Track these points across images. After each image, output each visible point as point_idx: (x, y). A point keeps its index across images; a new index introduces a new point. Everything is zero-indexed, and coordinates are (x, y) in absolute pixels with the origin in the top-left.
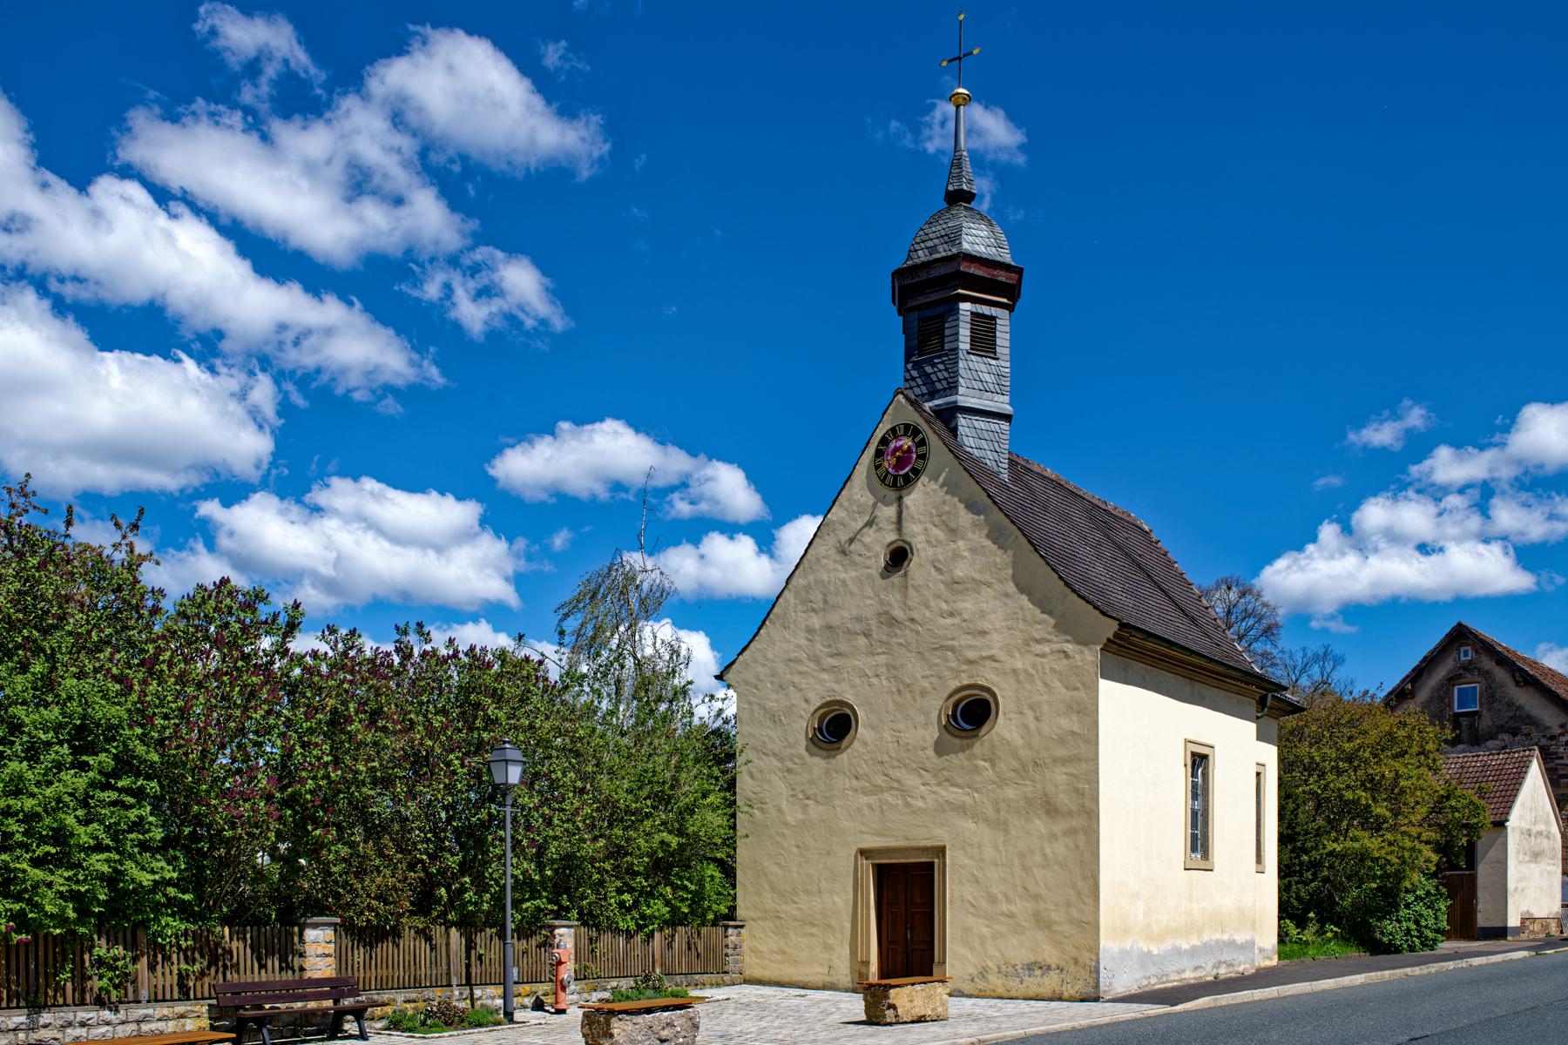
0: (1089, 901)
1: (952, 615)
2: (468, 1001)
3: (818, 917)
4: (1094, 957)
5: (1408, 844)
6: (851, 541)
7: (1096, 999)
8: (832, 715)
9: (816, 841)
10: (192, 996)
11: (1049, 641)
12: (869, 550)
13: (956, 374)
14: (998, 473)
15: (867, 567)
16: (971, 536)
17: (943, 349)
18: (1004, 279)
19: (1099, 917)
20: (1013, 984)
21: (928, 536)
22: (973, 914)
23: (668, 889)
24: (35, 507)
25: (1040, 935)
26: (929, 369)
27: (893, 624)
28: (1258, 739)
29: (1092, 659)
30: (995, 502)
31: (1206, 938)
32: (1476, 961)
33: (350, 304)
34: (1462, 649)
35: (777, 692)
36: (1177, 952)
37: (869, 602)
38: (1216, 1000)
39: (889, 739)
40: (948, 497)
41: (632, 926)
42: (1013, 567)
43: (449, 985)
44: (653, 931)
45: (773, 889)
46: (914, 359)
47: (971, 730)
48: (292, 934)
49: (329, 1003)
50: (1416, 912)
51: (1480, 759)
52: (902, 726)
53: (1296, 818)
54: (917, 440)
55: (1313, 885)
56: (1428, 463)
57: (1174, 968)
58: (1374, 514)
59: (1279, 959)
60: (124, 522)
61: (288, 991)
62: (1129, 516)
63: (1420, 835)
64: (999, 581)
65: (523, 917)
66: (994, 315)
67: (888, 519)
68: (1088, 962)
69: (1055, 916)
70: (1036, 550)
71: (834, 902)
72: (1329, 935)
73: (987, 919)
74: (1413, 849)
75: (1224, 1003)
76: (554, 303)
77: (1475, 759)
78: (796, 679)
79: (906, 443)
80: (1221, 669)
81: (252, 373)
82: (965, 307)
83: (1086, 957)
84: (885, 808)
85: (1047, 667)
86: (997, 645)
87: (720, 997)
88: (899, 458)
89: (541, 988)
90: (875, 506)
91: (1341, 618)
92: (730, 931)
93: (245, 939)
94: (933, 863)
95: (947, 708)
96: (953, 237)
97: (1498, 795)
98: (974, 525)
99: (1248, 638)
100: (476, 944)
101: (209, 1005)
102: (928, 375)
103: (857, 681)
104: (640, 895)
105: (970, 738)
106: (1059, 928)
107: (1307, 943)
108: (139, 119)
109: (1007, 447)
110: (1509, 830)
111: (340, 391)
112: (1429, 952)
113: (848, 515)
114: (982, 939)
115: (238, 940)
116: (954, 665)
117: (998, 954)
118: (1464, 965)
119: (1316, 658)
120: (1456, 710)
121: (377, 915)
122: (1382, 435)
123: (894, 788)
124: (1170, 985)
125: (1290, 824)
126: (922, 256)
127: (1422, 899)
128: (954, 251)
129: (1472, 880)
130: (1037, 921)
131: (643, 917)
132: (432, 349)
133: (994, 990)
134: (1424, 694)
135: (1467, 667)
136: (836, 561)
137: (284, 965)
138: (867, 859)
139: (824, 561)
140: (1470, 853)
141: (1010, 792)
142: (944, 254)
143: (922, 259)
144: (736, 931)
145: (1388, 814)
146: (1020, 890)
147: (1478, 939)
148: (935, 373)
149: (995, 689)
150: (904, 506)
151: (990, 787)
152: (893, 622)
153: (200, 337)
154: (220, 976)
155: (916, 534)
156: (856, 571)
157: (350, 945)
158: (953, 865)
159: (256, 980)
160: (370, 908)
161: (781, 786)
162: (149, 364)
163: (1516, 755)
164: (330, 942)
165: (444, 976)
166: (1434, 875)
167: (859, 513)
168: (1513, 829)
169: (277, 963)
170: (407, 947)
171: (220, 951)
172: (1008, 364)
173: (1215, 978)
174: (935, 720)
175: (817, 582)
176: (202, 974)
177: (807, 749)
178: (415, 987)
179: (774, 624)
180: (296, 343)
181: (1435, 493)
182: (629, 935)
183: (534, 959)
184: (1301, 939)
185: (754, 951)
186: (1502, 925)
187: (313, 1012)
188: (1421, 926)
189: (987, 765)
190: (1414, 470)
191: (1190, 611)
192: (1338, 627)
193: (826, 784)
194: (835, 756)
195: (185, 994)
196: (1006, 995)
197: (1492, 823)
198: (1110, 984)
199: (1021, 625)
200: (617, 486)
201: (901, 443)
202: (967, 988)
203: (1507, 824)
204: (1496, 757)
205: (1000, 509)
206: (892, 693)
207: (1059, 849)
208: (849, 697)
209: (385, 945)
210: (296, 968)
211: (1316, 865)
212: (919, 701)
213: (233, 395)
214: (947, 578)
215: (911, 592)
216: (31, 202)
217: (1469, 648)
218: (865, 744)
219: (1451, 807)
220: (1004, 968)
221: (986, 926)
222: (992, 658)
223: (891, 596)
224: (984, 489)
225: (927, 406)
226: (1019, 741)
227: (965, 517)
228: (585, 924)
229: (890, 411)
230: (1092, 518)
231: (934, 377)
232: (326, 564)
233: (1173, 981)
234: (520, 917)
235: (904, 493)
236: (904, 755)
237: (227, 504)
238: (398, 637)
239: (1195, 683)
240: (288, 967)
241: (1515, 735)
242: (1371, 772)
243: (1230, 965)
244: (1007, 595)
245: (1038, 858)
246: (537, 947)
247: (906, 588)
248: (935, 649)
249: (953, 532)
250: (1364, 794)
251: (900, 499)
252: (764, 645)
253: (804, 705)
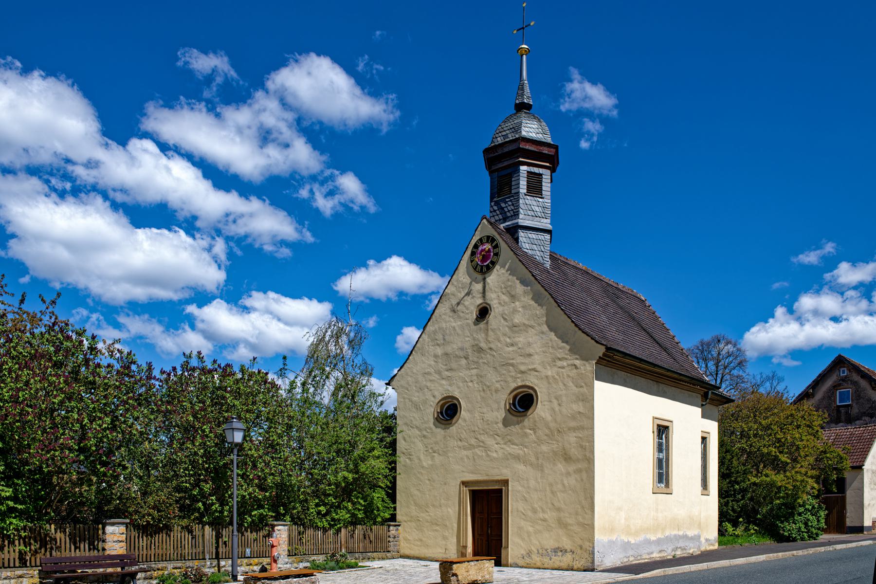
0: (589, 512)
1: (512, 345)
2: (216, 568)
3: (440, 520)
4: (591, 545)
5: (799, 478)
6: (458, 304)
7: (593, 570)
8: (448, 405)
9: (439, 476)
10: (28, 565)
11: (566, 359)
12: (467, 309)
13: (518, 207)
14: (543, 264)
15: (467, 319)
16: (523, 299)
17: (511, 193)
18: (547, 152)
19: (594, 521)
20: (546, 560)
21: (499, 300)
22: (523, 519)
23: (349, 504)
24: (6, 293)
25: (561, 532)
26: (503, 205)
27: (480, 351)
28: (702, 417)
29: (590, 369)
30: (536, 279)
31: (667, 533)
32: (839, 547)
33: (264, 200)
34: (841, 369)
35: (418, 392)
36: (648, 542)
37: (467, 339)
38: (665, 571)
39: (478, 418)
40: (511, 277)
41: (326, 524)
42: (546, 316)
43: (204, 559)
44: (340, 528)
45: (416, 504)
46: (495, 199)
47: (523, 412)
48: (98, 529)
49: (119, 569)
50: (805, 518)
51: (849, 430)
52: (485, 410)
53: (732, 464)
54: (493, 245)
55: (742, 502)
56: (835, 272)
57: (646, 552)
58: (807, 302)
59: (719, 545)
60: (48, 301)
61: (90, 562)
62: (632, 291)
63: (807, 472)
64: (539, 325)
65: (252, 520)
66: (541, 173)
67: (478, 291)
68: (588, 548)
69: (570, 521)
70: (559, 306)
71: (448, 512)
72: (752, 531)
73: (532, 523)
74: (803, 481)
75: (670, 573)
76: (370, 197)
77: (846, 431)
78: (429, 384)
79: (487, 246)
80: (676, 376)
81: (213, 238)
82: (524, 168)
83: (587, 545)
84: (476, 457)
85: (565, 374)
86: (537, 362)
87: (376, 566)
88: (483, 256)
89: (265, 561)
90: (471, 283)
91: (790, 356)
92: (391, 528)
93: (65, 532)
94: (502, 489)
95: (509, 399)
96: (517, 129)
97: (858, 450)
98: (525, 292)
99: (729, 368)
100: (222, 535)
101: (39, 570)
102: (503, 208)
103: (461, 384)
104: (331, 507)
105: (522, 416)
106: (572, 528)
107: (737, 536)
108: (150, 107)
109: (549, 249)
110: (865, 470)
111: (257, 246)
112: (813, 541)
113: (456, 289)
114: (528, 533)
115: (60, 532)
116: (513, 374)
117: (538, 543)
118: (831, 549)
119: (768, 379)
120: (838, 404)
121: (153, 518)
122: (811, 258)
123: (480, 446)
124: (643, 561)
125: (728, 467)
126: (500, 140)
127: (809, 511)
128: (517, 136)
129: (843, 499)
130: (559, 523)
131: (333, 519)
132: (306, 223)
133: (535, 564)
134: (819, 395)
135: (844, 379)
136: (450, 316)
137: (92, 547)
138: (466, 487)
139: (443, 317)
140: (841, 484)
141: (544, 448)
142: (511, 138)
143: (499, 142)
144: (395, 528)
145: (789, 461)
146: (550, 505)
147: (847, 533)
148: (506, 207)
149: (536, 388)
150: (487, 283)
151: (533, 445)
152: (480, 350)
153: (186, 220)
154: (48, 553)
155: (493, 299)
156: (460, 321)
157: (137, 535)
158: (512, 491)
159: (73, 555)
160: (149, 515)
161: (420, 445)
162: (161, 234)
163: (870, 428)
164: (123, 533)
165: (201, 553)
166: (817, 497)
167: (462, 288)
168: (868, 470)
169: (87, 546)
170: (175, 537)
171: (48, 539)
172: (549, 201)
173: (674, 557)
174: (503, 406)
175: (440, 328)
176: (36, 552)
177: (434, 424)
178: (181, 560)
179: (417, 353)
180: (234, 222)
181: (839, 290)
182: (325, 530)
183: (262, 544)
184: (734, 534)
185: (406, 539)
186: (860, 525)
187: (111, 574)
188: (808, 526)
189: (531, 432)
190: (827, 276)
191: (667, 346)
192: (789, 363)
193: (444, 444)
194: (449, 428)
195: (23, 563)
196: (541, 567)
197: (851, 467)
198: (602, 561)
199: (551, 350)
200: (401, 294)
201: (485, 247)
202: (521, 562)
203: (864, 467)
204: (858, 429)
205: (539, 283)
206: (480, 391)
207: (572, 481)
208: (457, 394)
209: (161, 536)
210: (100, 548)
211: (744, 491)
212: (494, 396)
213: (204, 249)
214: (510, 324)
215: (490, 333)
216: (100, 154)
217: (845, 369)
218: (465, 420)
219: (827, 458)
220: (540, 551)
221: (531, 526)
222: (535, 370)
223: (479, 335)
224: (530, 271)
225: (502, 226)
226: (549, 418)
227: (520, 288)
228: (295, 524)
229: (479, 229)
230: (605, 291)
231: (506, 210)
232: (252, 337)
233: (645, 558)
234: (250, 520)
235: (486, 275)
236: (486, 427)
237: (200, 306)
238: (185, 360)
239: (660, 384)
240: (94, 549)
241: (872, 417)
242: (779, 437)
243: (683, 549)
244: (543, 333)
245: (560, 486)
246: (263, 537)
247: (487, 330)
248: (504, 365)
249: (513, 297)
250: (774, 449)
251: (484, 279)
252: (412, 366)
253: (432, 399)
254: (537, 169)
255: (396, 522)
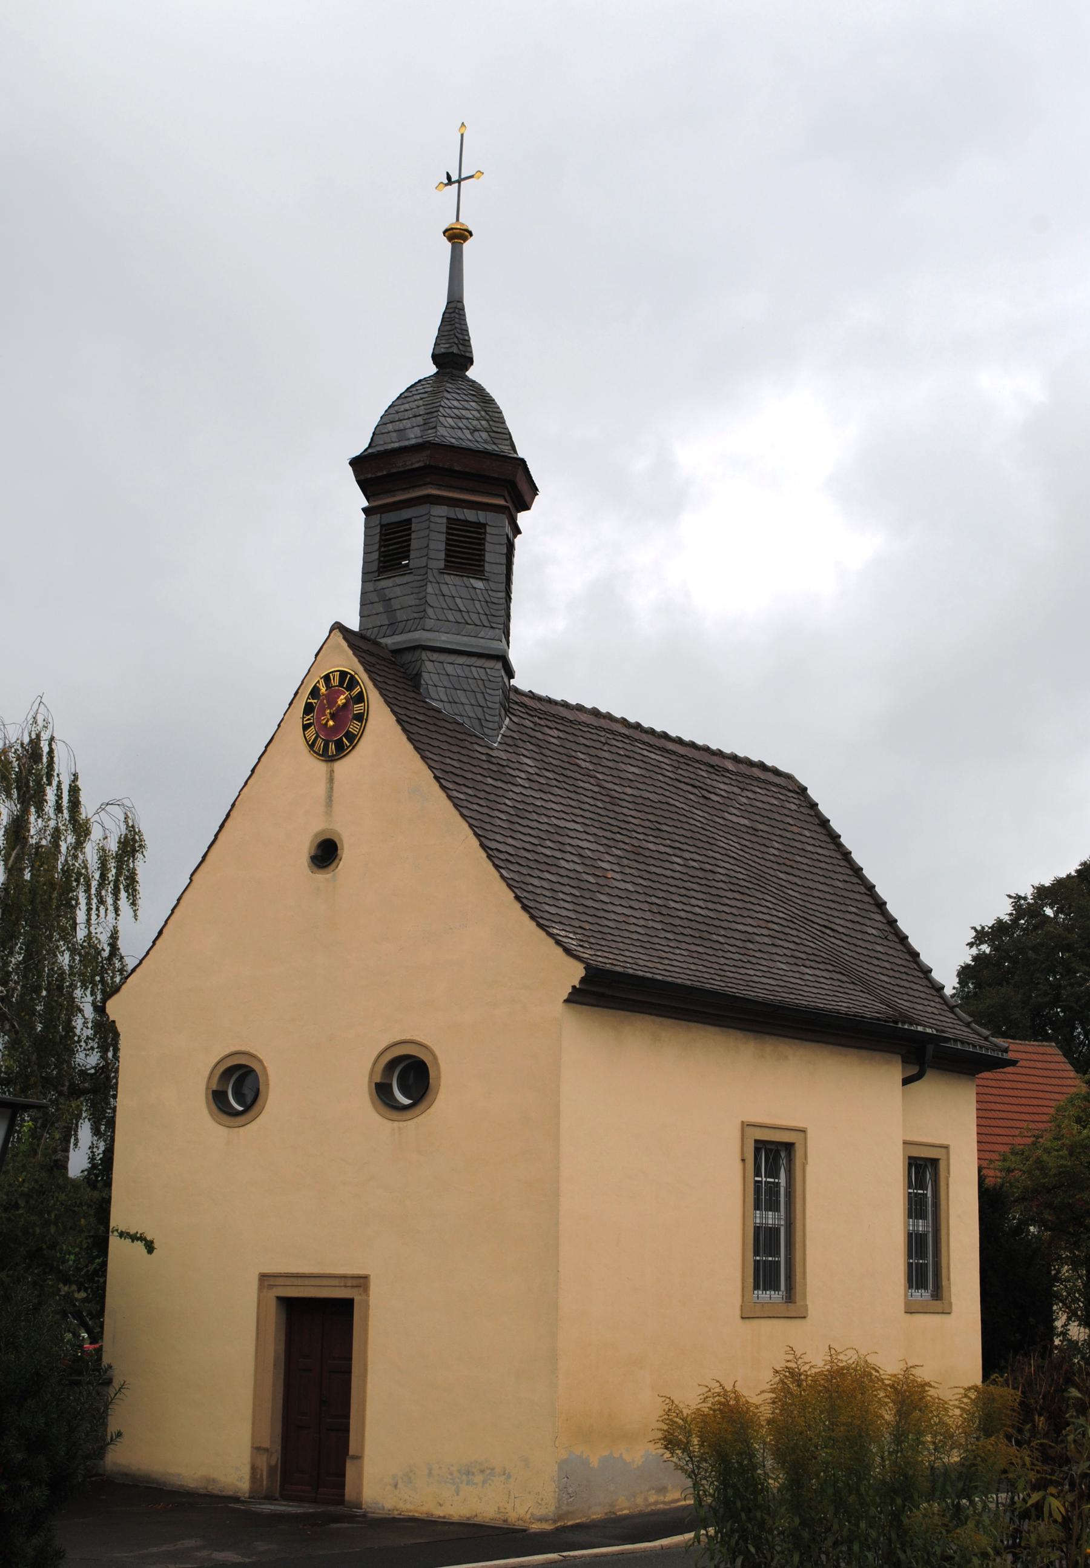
66: (483, 521)
254: (474, 512)
255: (778, 1230)
